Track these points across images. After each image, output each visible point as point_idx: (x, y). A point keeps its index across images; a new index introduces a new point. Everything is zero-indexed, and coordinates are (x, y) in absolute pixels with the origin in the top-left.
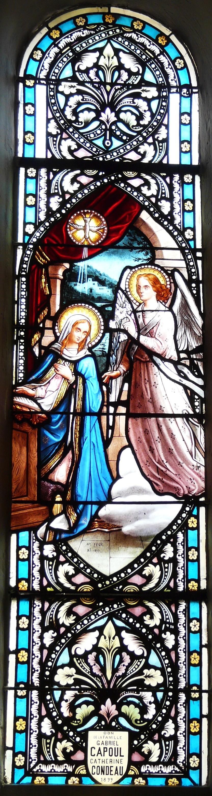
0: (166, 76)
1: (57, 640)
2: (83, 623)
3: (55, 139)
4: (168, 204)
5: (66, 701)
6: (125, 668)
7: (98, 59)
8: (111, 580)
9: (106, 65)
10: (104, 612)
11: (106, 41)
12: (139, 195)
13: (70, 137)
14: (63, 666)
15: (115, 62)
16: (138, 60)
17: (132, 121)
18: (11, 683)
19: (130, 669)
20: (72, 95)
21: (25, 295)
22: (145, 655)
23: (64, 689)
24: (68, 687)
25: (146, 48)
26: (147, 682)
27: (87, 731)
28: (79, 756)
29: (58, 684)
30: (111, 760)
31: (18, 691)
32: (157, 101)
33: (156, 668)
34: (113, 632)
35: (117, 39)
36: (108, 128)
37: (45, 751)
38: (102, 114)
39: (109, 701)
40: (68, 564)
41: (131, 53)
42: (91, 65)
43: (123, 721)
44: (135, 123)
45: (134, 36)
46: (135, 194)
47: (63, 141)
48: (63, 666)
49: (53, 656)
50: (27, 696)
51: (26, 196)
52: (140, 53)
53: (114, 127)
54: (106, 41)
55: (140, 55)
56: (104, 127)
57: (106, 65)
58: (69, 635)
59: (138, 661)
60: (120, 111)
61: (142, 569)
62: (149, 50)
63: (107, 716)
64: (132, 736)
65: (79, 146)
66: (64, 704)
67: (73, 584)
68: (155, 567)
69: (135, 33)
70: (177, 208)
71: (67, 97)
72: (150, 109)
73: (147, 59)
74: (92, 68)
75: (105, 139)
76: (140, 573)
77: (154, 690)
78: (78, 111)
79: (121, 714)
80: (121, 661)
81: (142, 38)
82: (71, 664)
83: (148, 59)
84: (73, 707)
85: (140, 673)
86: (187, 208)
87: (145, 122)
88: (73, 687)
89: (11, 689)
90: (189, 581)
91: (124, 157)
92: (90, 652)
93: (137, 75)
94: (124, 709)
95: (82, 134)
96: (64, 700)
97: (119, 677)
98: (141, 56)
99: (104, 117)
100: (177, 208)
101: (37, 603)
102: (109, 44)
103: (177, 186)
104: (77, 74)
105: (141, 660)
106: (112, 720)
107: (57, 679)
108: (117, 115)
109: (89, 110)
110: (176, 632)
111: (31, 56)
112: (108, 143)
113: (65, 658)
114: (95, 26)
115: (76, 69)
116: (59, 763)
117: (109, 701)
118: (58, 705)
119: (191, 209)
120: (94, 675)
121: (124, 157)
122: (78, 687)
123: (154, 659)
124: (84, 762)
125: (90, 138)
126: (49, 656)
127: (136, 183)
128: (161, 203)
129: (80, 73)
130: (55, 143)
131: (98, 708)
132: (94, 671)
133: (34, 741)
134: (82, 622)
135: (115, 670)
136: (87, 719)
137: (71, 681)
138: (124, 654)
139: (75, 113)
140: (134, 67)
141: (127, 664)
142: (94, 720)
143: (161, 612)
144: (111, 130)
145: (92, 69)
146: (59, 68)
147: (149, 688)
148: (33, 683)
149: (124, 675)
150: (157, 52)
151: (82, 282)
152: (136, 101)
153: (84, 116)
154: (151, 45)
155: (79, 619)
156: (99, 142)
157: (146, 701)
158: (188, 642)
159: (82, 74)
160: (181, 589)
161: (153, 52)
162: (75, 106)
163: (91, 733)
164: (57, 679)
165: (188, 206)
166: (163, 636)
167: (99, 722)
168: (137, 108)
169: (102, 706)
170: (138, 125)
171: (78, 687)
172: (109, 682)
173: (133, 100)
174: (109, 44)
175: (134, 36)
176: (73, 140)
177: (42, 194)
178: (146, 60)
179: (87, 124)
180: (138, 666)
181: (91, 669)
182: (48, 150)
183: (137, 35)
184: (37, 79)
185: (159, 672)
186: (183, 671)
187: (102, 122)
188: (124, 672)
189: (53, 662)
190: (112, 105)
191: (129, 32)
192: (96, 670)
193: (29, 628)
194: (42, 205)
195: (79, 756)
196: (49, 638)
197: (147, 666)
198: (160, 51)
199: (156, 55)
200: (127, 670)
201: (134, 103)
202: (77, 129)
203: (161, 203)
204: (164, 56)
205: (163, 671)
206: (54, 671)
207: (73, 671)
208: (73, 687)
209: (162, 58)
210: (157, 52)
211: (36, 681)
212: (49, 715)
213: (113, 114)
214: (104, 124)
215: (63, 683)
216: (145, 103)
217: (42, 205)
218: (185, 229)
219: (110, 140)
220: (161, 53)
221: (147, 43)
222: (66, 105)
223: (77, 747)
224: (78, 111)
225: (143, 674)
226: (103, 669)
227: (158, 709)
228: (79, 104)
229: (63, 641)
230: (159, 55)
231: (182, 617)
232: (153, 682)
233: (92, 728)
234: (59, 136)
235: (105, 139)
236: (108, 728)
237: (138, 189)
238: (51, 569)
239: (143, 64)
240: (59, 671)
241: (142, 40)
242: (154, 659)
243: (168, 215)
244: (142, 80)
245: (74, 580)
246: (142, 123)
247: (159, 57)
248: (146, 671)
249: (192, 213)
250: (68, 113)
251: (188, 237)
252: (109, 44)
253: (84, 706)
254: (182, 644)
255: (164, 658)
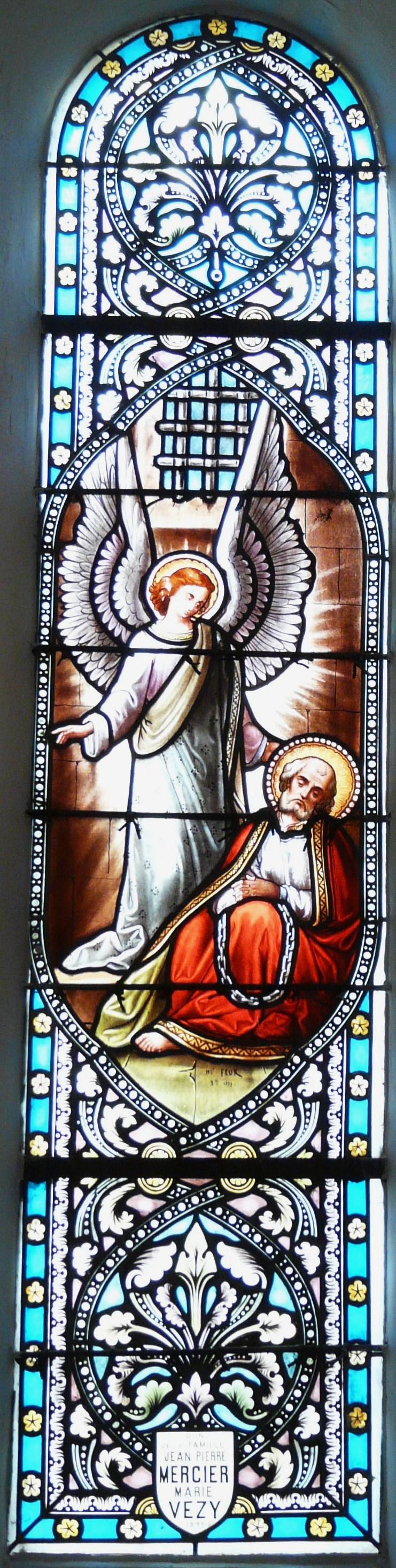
0: (327, 140)
1: (98, 1262)
2: (149, 1227)
3: (115, 272)
4: (325, 403)
5: (145, 207)
6: (226, 1311)
7: (175, 1258)
8: (204, 1130)
9: (191, 1274)
10: (190, 1206)
11: (191, 1218)
12: (269, 386)
13: (121, 1100)
14: (109, 1311)
15: (209, 1266)
16: (276, 108)
17: (246, 1397)
18: (52, 158)
19: (235, 1314)
20: (147, 183)
21: (49, 621)
22: (264, 1286)
23: (112, 1352)
24: (120, 1349)
25: (290, 85)
26: (265, 1338)
27: (153, 1432)
28: (140, 1479)
29: (103, 1343)
30: (197, 1490)
31: (62, 169)
32: (310, 189)
33: (281, 1311)
34: (204, 1245)
35: (213, 1212)
36: (217, 246)
37: (83, 1122)
38: (184, 1386)
39: (196, 1378)
40: (123, 1105)
41: (243, 1244)
42: (158, 1276)
43: (222, 1411)
44: (251, 1404)
45: (267, 60)
46: (262, 383)
47: (107, 1108)
48: (109, 1311)
49: (92, 1291)
50: (78, 179)
51: (60, 213)
52: (262, 1241)
53: (225, 246)
54: (191, 1218)
55: (261, 1245)
56: (207, 244)
57: (191, 1274)
58: (121, 1252)
59: (249, 1297)
60: (238, 212)
61: (263, 1112)
62: (296, 88)
63: (194, 1406)
64: (240, 1439)
65: (162, 284)
66: (113, 1381)
67: (132, 1143)
68: (286, 1107)
69: (269, 54)
70: (342, 414)
71: (140, 188)
72: (283, 1372)
73: (275, 1255)
74: (186, 129)
75: (211, 268)
76: (258, 1117)
77: (278, 1351)
78: (158, 216)
79: (220, 1399)
80: (219, 1298)
81: (284, 65)
82: (126, 1307)
83: (277, 1253)
84: (129, 1389)
85: (253, 1320)
86: (361, 412)
87: (272, 1400)
88: (130, 1349)
89: (52, 165)
90: (349, 1138)
91: (247, 300)
92: (161, 1283)
93: (255, 1292)
94: (225, 1389)
95: (164, 259)
96: (140, 206)
97: (217, 1327)
98: (264, 1248)
99: (185, 1396)
100: (342, 414)
101: (64, 1153)
102: (197, 1225)
103: (342, 370)
104: (158, 140)
105: (255, 1295)
106: (204, 1411)
107: (99, 1334)
108: (233, 222)
109: (182, 213)
110: (320, 1241)
111: (68, 119)
112: (217, 276)
113: (113, 1295)
114: (192, 42)
115: (129, 1286)
116: (103, 1493)
117: (196, 1378)
118: (103, 1385)
119: (369, 413)
120: (168, 1324)
121: (247, 300)
122: (138, 1349)
123: (279, 1295)
124: (149, 1491)
125: (182, 266)
126: (83, 1291)
127: (264, 362)
128: (300, 1248)
129: (138, 1294)
130: (114, 280)
131: (177, 1390)
132: (168, 1318)
133: (56, 1453)
134: (148, 1224)
135: (206, 1317)
136: (156, 1408)
137: (125, 1339)
138: (225, 1285)
139: (154, 219)
140: (250, 1274)
141: (230, 1306)
142: (169, 1411)
143: (294, 1207)
144: (222, 254)
145: (163, 1285)
146: (91, 1300)
147: (268, 1347)
148: (52, 1347)
149: (225, 1325)
150: (311, 91)
151: (157, 614)
152: (271, 189)
153: (169, 227)
154: (301, 79)
155: (140, 1220)
156: (200, 274)
157: (265, 1373)
158: (344, 1258)
159: (141, 1297)
160: (334, 1154)
161: (302, 92)
162: (154, 206)
163: (160, 1435)
164: (99, 1334)
165: (356, 1229)
166: (297, 1250)
167: (179, 1413)
168: (271, 203)
169: (184, 1386)
170: (259, 1406)
171: (138, 1349)
172: (196, 1339)
173: (265, 189)
174: (197, 1224)
175: (267, 60)
176: (128, 1106)
177: (84, 386)
178: (273, 1257)
179: (177, 238)
180: (251, 1306)
181: (164, 1314)
182: (100, 358)
183: (274, 58)
184: (80, 164)
185: (287, 1318)
186: (334, 1313)
187: (203, 237)
188: (225, 1319)
189: (91, 1304)
190: (223, 202)
191: (257, 54)
192: (173, 1315)
193: (45, 1241)
194: (84, 406)
195: (140, 1479)
196: (83, 1257)
197: (266, 1307)
198: (317, 89)
199: (310, 97)
200: (229, 1316)
201: (267, 194)
202: (155, 249)
203: (300, 1248)
204: (326, 99)
205: (296, 1318)
206: (94, 1320)
207: (130, 1317)
208: (130, 1349)
209: (321, 104)
210: (311, 91)
211: (59, 1343)
212: (85, 1400)
213: (227, 218)
214: (207, 238)
215: (112, 1342)
216: (289, 193)
217: (84, 406)
218: (356, 453)
219: (221, 269)
220: (320, 94)
221: (292, 74)
222: (136, 203)
223: (137, 1461)
224: (158, 216)
225: (257, 1322)
226: (186, 1317)
227: (288, 1385)
228: (162, 202)
229: (110, 1263)
230: (314, 97)
231: (333, 1216)
232: (276, 1338)
233: (163, 1428)
234: (123, 268)
235: (211, 268)
236: (196, 1425)
237: (268, 375)
238: (116, 283)
239: (284, 116)
240: (104, 1319)
241: (282, 68)
242: (279, 1295)
243: (324, 424)
244: (283, 151)
245: (133, 1135)
246: (266, 1401)
247: (314, 102)
248: (262, 1318)
249: (366, 1101)
250: (141, 220)
251: (362, 468)
252: (197, 1224)
253: (175, 217)
254: (334, 1264)
255: (299, 1294)
